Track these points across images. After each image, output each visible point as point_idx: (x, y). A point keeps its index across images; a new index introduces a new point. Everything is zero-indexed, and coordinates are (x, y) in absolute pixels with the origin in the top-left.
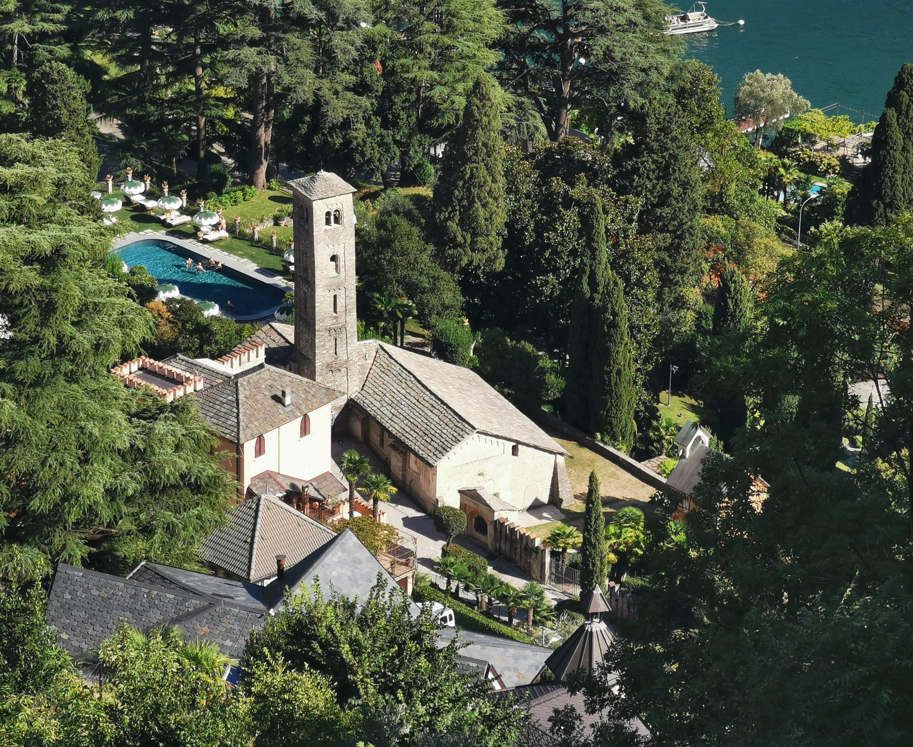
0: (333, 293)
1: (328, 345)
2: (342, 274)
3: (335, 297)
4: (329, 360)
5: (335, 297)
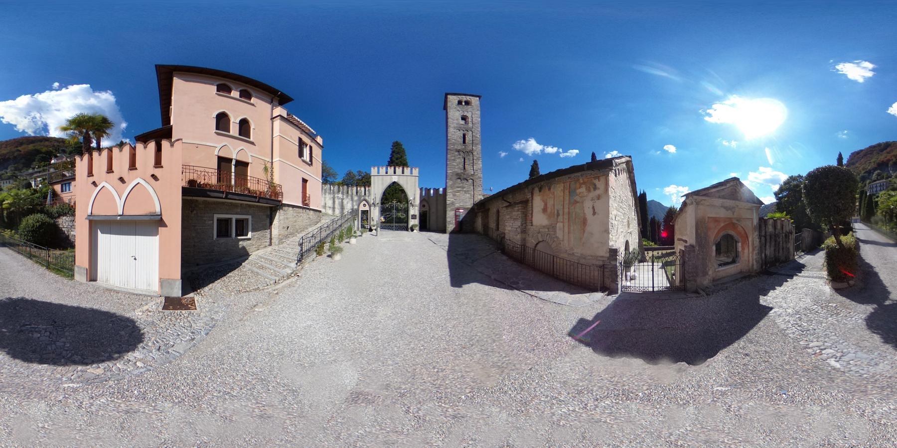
0: (462, 132)
1: (458, 160)
2: (470, 125)
3: (464, 136)
4: (460, 171)
5: (464, 136)
